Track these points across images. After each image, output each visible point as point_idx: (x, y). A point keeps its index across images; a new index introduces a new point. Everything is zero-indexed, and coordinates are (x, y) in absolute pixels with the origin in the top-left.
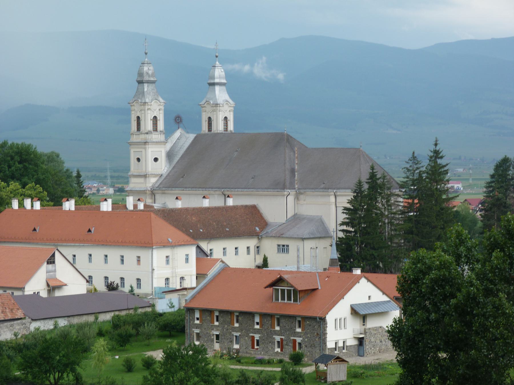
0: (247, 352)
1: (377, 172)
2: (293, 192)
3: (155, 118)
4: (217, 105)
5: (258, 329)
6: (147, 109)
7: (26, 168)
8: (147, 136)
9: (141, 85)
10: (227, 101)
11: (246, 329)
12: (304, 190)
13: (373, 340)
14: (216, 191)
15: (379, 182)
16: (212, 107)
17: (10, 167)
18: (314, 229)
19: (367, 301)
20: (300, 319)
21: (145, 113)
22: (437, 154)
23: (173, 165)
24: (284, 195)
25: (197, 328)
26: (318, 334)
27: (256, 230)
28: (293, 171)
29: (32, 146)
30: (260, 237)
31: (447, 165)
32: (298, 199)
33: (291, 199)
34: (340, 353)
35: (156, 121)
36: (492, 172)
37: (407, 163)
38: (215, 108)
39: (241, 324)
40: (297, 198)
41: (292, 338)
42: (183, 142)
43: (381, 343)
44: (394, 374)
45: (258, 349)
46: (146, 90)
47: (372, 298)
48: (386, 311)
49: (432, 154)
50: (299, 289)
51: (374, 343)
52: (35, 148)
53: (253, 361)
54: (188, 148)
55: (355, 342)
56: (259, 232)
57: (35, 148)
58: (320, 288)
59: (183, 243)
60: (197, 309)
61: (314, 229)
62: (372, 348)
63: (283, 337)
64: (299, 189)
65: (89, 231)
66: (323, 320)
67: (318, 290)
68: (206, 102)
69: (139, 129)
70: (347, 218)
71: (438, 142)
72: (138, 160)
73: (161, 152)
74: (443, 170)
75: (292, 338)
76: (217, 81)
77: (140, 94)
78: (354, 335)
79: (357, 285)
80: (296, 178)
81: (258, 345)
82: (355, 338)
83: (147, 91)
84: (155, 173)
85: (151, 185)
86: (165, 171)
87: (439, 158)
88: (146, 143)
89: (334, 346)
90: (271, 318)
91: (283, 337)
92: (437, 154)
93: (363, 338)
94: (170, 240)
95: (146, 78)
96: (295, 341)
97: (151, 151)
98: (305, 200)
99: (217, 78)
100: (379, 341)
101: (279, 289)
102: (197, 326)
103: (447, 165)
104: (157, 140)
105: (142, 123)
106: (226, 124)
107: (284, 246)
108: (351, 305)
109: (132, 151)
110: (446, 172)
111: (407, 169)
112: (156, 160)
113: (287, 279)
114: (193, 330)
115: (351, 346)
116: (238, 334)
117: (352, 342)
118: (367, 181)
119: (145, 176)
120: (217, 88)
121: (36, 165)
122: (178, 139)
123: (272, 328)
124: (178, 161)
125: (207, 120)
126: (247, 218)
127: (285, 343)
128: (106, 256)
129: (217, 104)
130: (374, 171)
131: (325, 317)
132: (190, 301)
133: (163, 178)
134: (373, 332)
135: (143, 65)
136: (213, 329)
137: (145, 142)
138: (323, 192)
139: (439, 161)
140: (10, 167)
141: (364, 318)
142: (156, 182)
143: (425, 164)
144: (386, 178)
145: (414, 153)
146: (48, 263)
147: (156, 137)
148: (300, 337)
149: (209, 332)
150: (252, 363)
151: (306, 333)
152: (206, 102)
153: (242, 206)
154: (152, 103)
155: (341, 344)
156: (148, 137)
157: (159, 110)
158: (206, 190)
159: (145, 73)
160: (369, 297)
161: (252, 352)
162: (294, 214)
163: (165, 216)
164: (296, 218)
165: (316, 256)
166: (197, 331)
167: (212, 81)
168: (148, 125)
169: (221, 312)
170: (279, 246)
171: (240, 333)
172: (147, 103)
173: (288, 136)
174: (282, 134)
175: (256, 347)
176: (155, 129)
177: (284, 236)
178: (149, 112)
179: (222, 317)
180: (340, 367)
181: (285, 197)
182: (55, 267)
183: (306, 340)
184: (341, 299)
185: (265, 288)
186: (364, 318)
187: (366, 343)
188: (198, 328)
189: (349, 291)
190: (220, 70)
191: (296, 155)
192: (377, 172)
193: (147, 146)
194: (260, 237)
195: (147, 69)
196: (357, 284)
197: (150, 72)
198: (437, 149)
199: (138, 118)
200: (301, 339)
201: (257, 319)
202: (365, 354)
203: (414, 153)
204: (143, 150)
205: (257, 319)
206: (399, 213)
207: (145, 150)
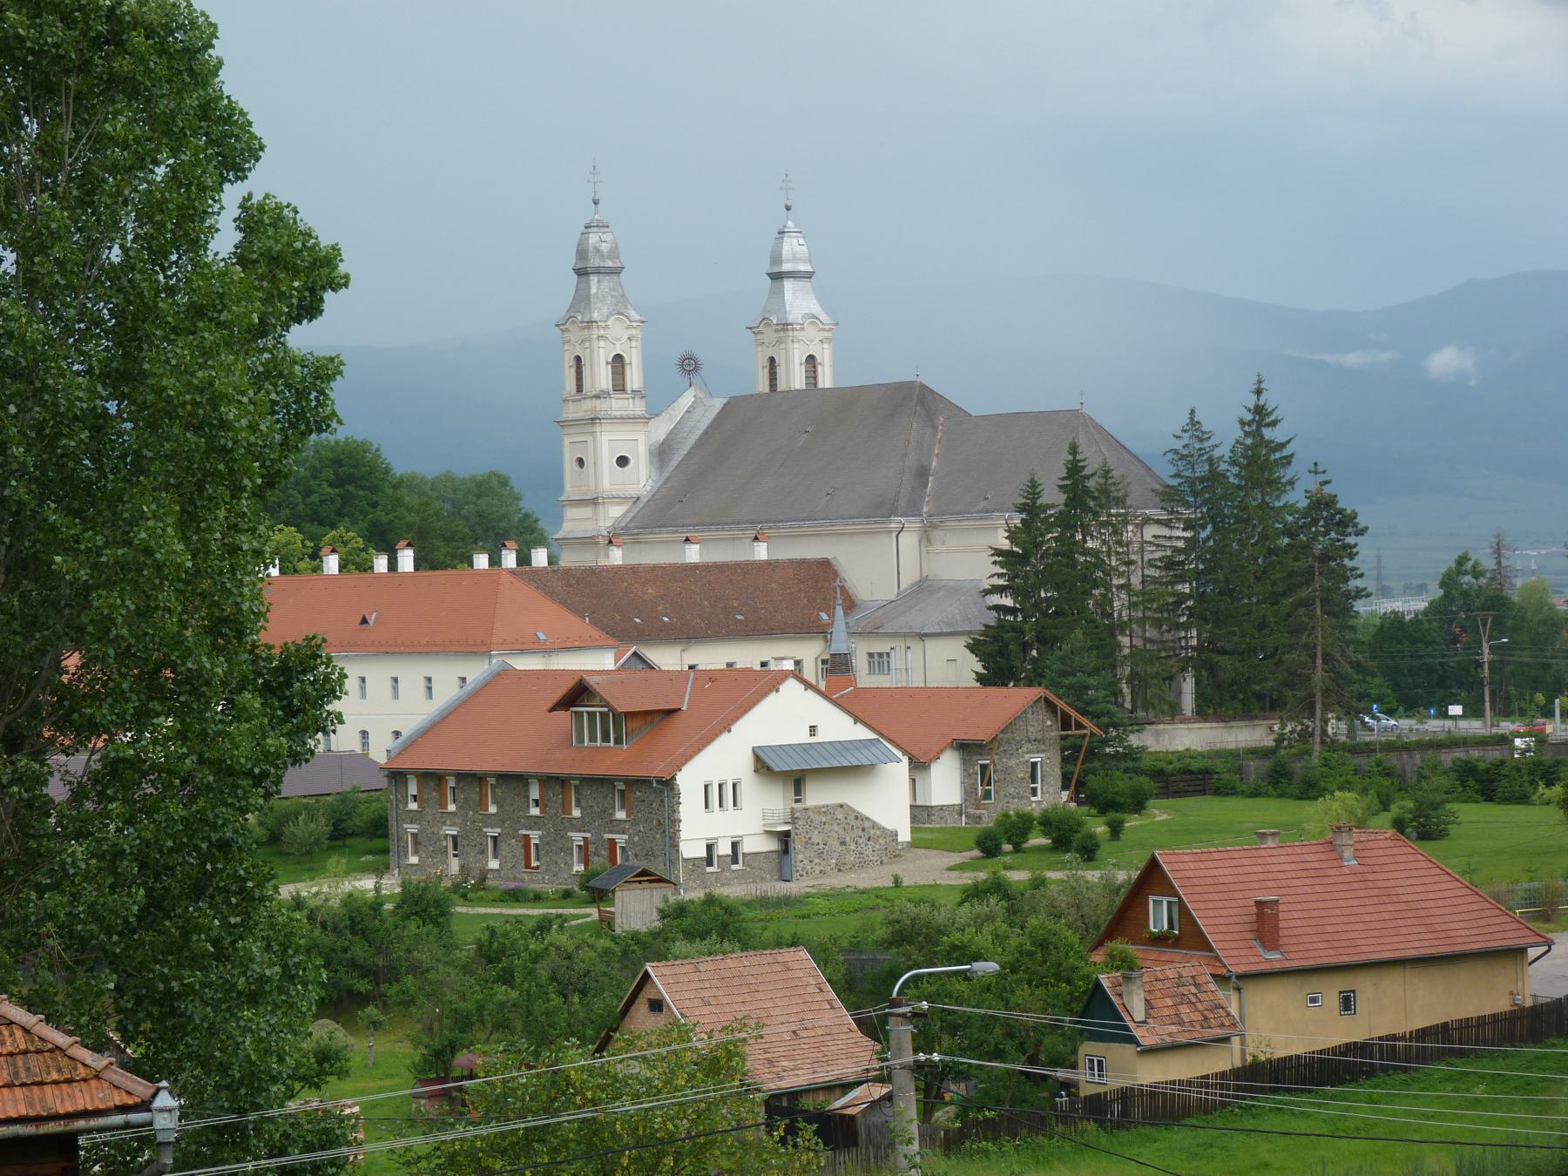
0: (515, 878)
1: (1084, 460)
2: (913, 524)
3: (618, 358)
4: (785, 326)
5: (537, 817)
7: (347, 498)
8: (597, 402)
9: (584, 278)
10: (813, 316)
11: (512, 818)
12: (940, 518)
13: (816, 838)
14: (746, 529)
15: (1091, 484)
16: (776, 331)
18: (956, 611)
19: (804, 738)
21: (591, 348)
22: (1261, 416)
23: (666, 474)
24: (891, 532)
26: (659, 823)
28: (922, 474)
29: (371, 444)
31: (1289, 442)
32: (929, 540)
33: (909, 540)
34: (723, 871)
35: (623, 366)
37: (1178, 437)
38: (782, 334)
39: (500, 806)
40: (926, 535)
41: (607, 836)
43: (843, 848)
44: (809, 917)
45: (537, 868)
46: (593, 290)
47: (820, 730)
48: (866, 762)
49: (1249, 417)
50: (621, 708)
51: (821, 846)
52: (378, 450)
53: (496, 895)
54: (706, 432)
55: (772, 845)
57: (378, 450)
58: (684, 708)
59: (577, 644)
61: (956, 611)
62: (816, 861)
63: (588, 835)
64: (930, 515)
65: (364, 621)
69: (579, 388)
70: (1000, 575)
71: (1262, 386)
72: (581, 462)
73: (640, 443)
74: (1278, 455)
75: (607, 836)
76: (786, 267)
77: (582, 300)
78: (765, 825)
79: (773, 697)
81: (538, 859)
82: (767, 832)
83: (596, 293)
84: (621, 494)
85: (609, 523)
86: (648, 488)
87: (1268, 425)
88: (593, 420)
89: (704, 854)
90: (563, 787)
91: (588, 835)
92: (1261, 416)
93: (787, 834)
94: (542, 636)
95: (594, 262)
96: (612, 843)
97: (608, 442)
98: (943, 543)
99: (788, 261)
100: (836, 843)
101: (582, 713)
102: (414, 817)
103: (1289, 442)
104: (624, 413)
105: (586, 371)
106: (812, 374)
107: (881, 655)
108: (754, 750)
109: (567, 441)
110: (1288, 460)
111: (1176, 452)
112: (623, 461)
113: (595, 686)
114: (405, 826)
115: (756, 854)
117: (755, 844)
118: (1062, 483)
119: (594, 502)
121: (374, 489)
123: (564, 812)
125: (767, 364)
126: (799, 591)
127: (592, 849)
128: (396, 680)
130: (1078, 457)
131: (673, 778)
133: (640, 505)
134: (817, 819)
136: (444, 823)
140: (308, 493)
141: (797, 781)
142: (624, 516)
145: (1192, 412)
148: (623, 833)
149: (435, 829)
150: (494, 901)
151: (635, 823)
153: (791, 561)
155: (724, 849)
156: (601, 405)
158: (723, 530)
161: (526, 877)
162: (918, 578)
163: (571, 586)
164: (924, 587)
165: (907, 670)
166: (412, 828)
167: (776, 270)
168: (602, 377)
169: (462, 776)
170: (871, 655)
171: (499, 830)
173: (924, 388)
174: (910, 386)
175: (534, 864)
176: (619, 385)
177: (881, 631)
178: (602, 344)
180: (652, 896)
181: (894, 535)
183: (636, 839)
184: (721, 732)
185: (551, 710)
186: (797, 781)
187: (797, 844)
189: (746, 711)
190: (795, 240)
191: (939, 435)
192: (1084, 460)
193: (598, 428)
196: (773, 696)
198: (1262, 402)
199: (578, 359)
200: (626, 837)
202: (795, 876)
203: (1192, 412)
204: (589, 438)
206: (1159, 564)
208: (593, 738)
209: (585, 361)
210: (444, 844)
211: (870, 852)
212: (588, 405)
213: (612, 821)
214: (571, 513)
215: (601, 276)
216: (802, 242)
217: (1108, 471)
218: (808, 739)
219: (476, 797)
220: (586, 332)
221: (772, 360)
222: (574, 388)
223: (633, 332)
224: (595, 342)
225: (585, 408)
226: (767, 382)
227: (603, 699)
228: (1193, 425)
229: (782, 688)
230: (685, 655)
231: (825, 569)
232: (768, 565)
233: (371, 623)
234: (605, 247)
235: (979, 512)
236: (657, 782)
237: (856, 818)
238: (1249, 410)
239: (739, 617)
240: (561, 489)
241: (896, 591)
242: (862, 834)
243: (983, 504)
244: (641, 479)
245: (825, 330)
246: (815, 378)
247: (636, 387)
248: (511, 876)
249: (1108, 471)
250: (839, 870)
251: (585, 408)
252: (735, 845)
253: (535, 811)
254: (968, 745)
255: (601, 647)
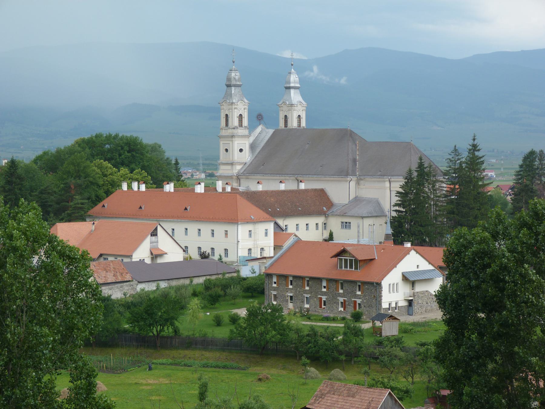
2: (354, 178)
3: (241, 115)
4: (292, 105)
5: (325, 292)
6: (234, 108)
7: (133, 156)
8: (234, 130)
9: (229, 88)
13: (420, 302)
14: (291, 177)
15: (426, 170)
16: (288, 106)
17: (120, 155)
19: (415, 269)
20: (360, 284)
21: (232, 112)
22: (475, 147)
25: (274, 291)
26: (374, 296)
27: (324, 210)
28: (355, 161)
30: (327, 215)
32: (358, 184)
33: (353, 184)
35: (242, 118)
36: (521, 162)
38: (290, 108)
39: (310, 288)
40: (358, 183)
41: (353, 299)
42: (264, 136)
45: (325, 308)
46: (233, 92)
47: (420, 267)
48: (431, 277)
49: (471, 148)
50: (360, 258)
52: (141, 140)
53: (321, 318)
54: (268, 141)
55: (405, 304)
56: (326, 211)
57: (141, 140)
58: (376, 258)
59: (263, 220)
60: (275, 274)
62: (420, 309)
63: (346, 299)
64: (359, 176)
65: (186, 209)
66: (379, 285)
67: (375, 260)
68: (283, 102)
69: (227, 125)
70: (400, 201)
71: (475, 138)
72: (227, 150)
73: (246, 144)
77: (229, 95)
80: (357, 167)
82: (405, 299)
83: (234, 93)
85: (236, 171)
86: (249, 160)
87: (477, 151)
88: (233, 136)
89: (388, 307)
91: (346, 299)
92: (475, 147)
93: (412, 300)
95: (233, 82)
96: (355, 302)
97: (237, 144)
98: (364, 185)
99: (292, 83)
100: (425, 303)
101: (342, 259)
102: (275, 289)
104: (242, 134)
107: (346, 223)
108: (402, 273)
109: (221, 143)
110: (483, 163)
111: (450, 159)
112: (241, 150)
114: (271, 292)
115: (402, 306)
116: (308, 296)
117: (403, 304)
118: (416, 169)
119: (232, 164)
120: (292, 91)
121: (142, 154)
122: (259, 133)
124: (260, 151)
127: (347, 303)
129: (292, 105)
130: (422, 161)
131: (381, 283)
132: (269, 268)
133: (247, 166)
134: (421, 295)
135: (231, 71)
136: (287, 292)
137: (232, 136)
138: (380, 178)
139: (477, 153)
140: (120, 155)
141: (413, 283)
142: (241, 169)
143: (465, 156)
144: (432, 167)
145: (455, 146)
146: (151, 236)
147: (241, 131)
148: (360, 299)
150: (320, 320)
151: (365, 296)
152: (283, 102)
153: (312, 189)
154: (238, 103)
155: (393, 305)
156: (235, 131)
157: (244, 109)
158: (282, 176)
159: (232, 78)
160: (418, 266)
164: (357, 200)
165: (373, 232)
166: (275, 293)
167: (288, 86)
168: (235, 122)
170: (342, 223)
172: (234, 103)
174: (346, 130)
175: (323, 307)
176: (241, 125)
177: (346, 214)
178: (236, 110)
179: (295, 281)
182: (158, 238)
183: (365, 301)
186: (413, 283)
187: (415, 304)
188: (276, 291)
190: (295, 76)
191: (358, 148)
193: (234, 139)
194: (327, 215)
195: (234, 75)
196: (408, 256)
197: (237, 77)
198: (475, 143)
199: (227, 115)
200: (361, 300)
201: (324, 284)
202: (414, 314)
203: (455, 146)
204: (231, 142)
205: (324, 284)
206: (443, 196)
207: (232, 142)
208: (346, 267)
209: (230, 116)
210: (287, 298)
211: (434, 306)
212: (230, 131)
213: (355, 295)
214: (222, 167)
215: (236, 87)
216: (297, 76)
217: (431, 166)
218: (417, 270)
219: (300, 284)
220: (230, 106)
221: (286, 116)
222: (225, 125)
223: (246, 107)
224: (234, 110)
225: (229, 132)
226: (284, 124)
227: (350, 254)
228: (455, 150)
229: (410, 253)
230: (284, 222)
231: (322, 192)
232: (306, 191)
233: (188, 210)
234: (237, 77)
235: (379, 176)
236: (376, 284)
237: (431, 295)
238: (470, 145)
239: (300, 209)
240: (219, 159)
241: (348, 201)
242: (432, 300)
243: (379, 173)
244: (247, 157)
245: (304, 107)
246: (300, 123)
247: (246, 125)
248: (314, 310)
249: (431, 166)
250: (426, 312)
251: (229, 132)
252: (396, 303)
253: (324, 290)
254: (442, 267)
255: (270, 221)
